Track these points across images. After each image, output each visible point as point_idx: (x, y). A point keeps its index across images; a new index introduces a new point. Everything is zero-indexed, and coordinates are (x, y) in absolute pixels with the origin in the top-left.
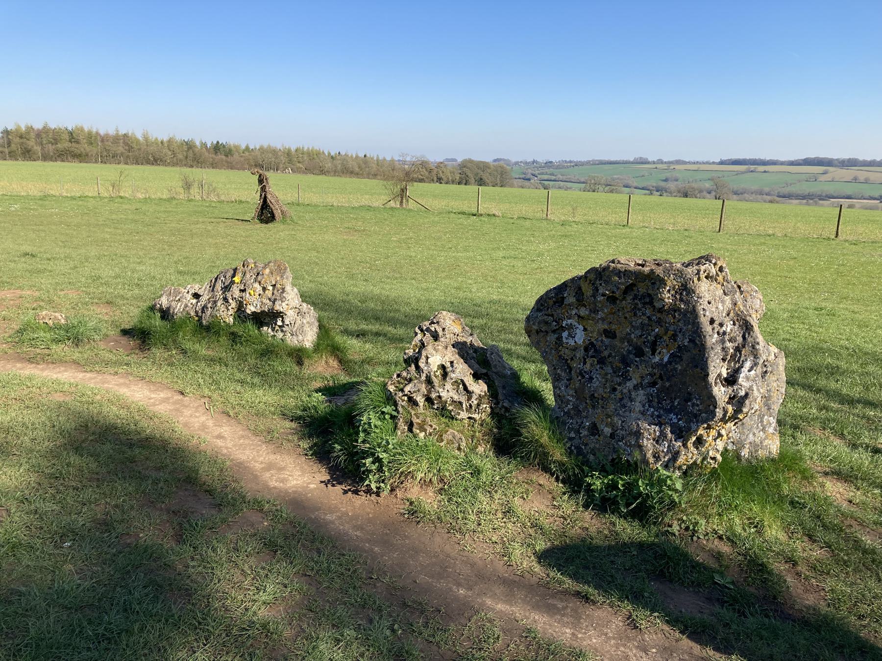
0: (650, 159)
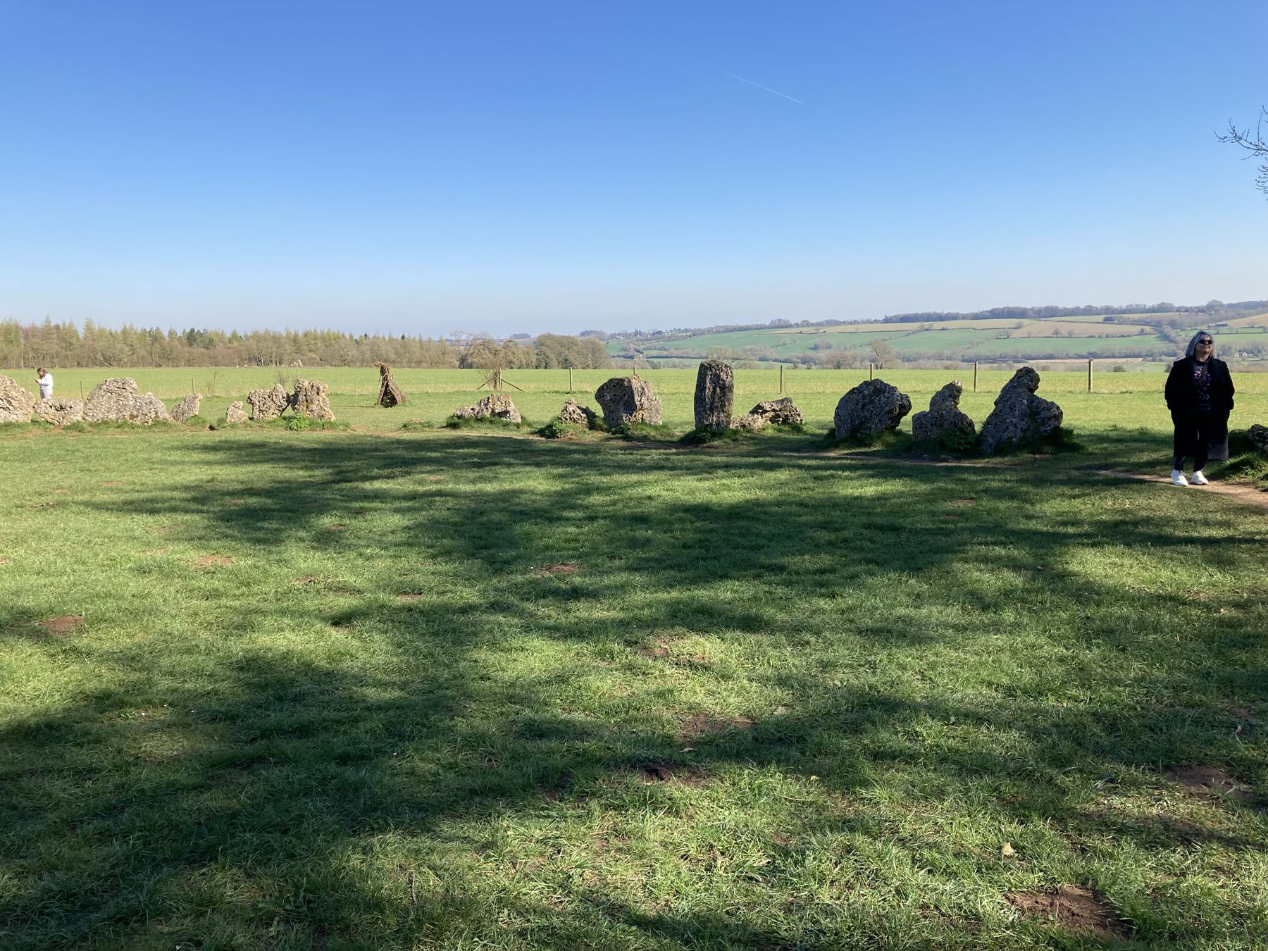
0: (792, 322)
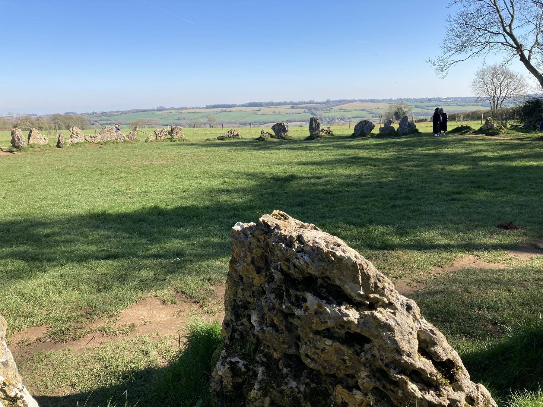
0: (167, 108)
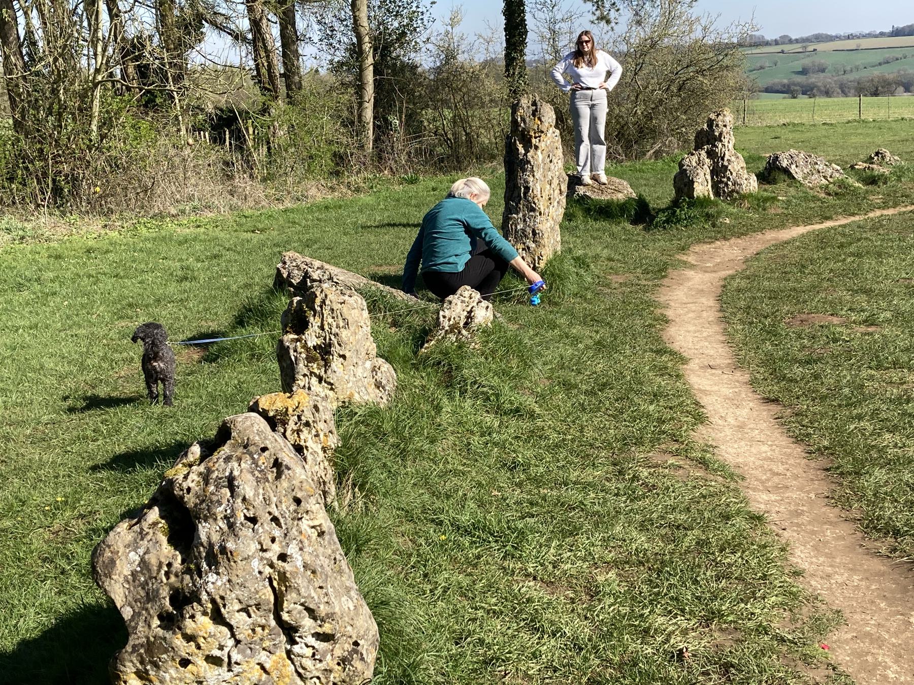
0: (768, 38)
